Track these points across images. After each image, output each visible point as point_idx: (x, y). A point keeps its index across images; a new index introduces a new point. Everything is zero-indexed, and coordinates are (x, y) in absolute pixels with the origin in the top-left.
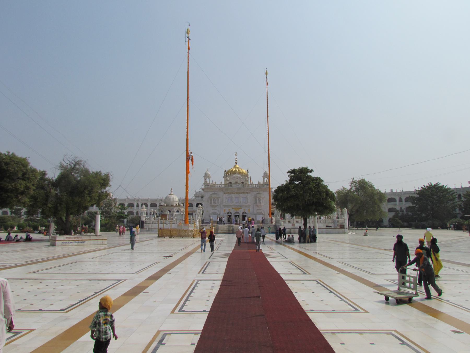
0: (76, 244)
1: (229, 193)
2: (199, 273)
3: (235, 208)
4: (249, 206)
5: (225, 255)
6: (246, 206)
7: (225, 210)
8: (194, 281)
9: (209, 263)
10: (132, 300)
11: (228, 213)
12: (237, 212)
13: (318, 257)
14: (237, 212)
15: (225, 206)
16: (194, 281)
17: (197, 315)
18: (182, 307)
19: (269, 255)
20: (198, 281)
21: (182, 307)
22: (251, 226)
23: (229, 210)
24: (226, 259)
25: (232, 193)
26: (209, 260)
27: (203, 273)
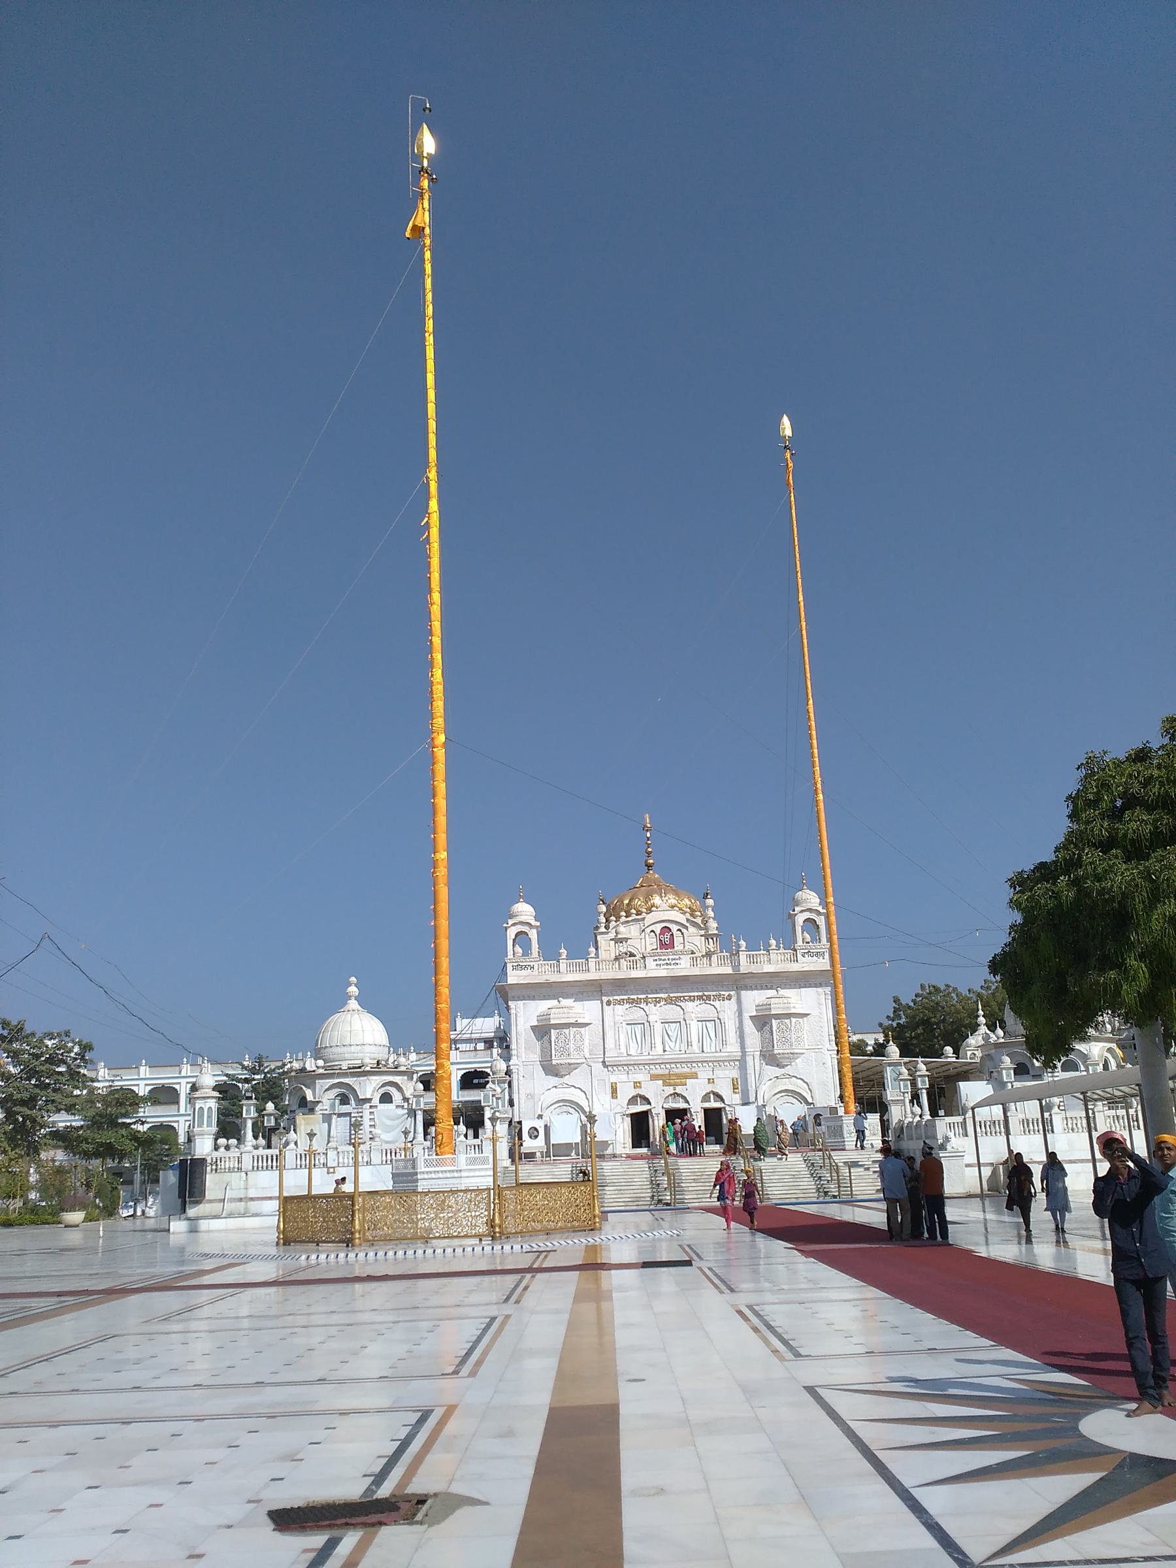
9: (507, 1300)
11: (632, 1101)
23: (637, 1085)
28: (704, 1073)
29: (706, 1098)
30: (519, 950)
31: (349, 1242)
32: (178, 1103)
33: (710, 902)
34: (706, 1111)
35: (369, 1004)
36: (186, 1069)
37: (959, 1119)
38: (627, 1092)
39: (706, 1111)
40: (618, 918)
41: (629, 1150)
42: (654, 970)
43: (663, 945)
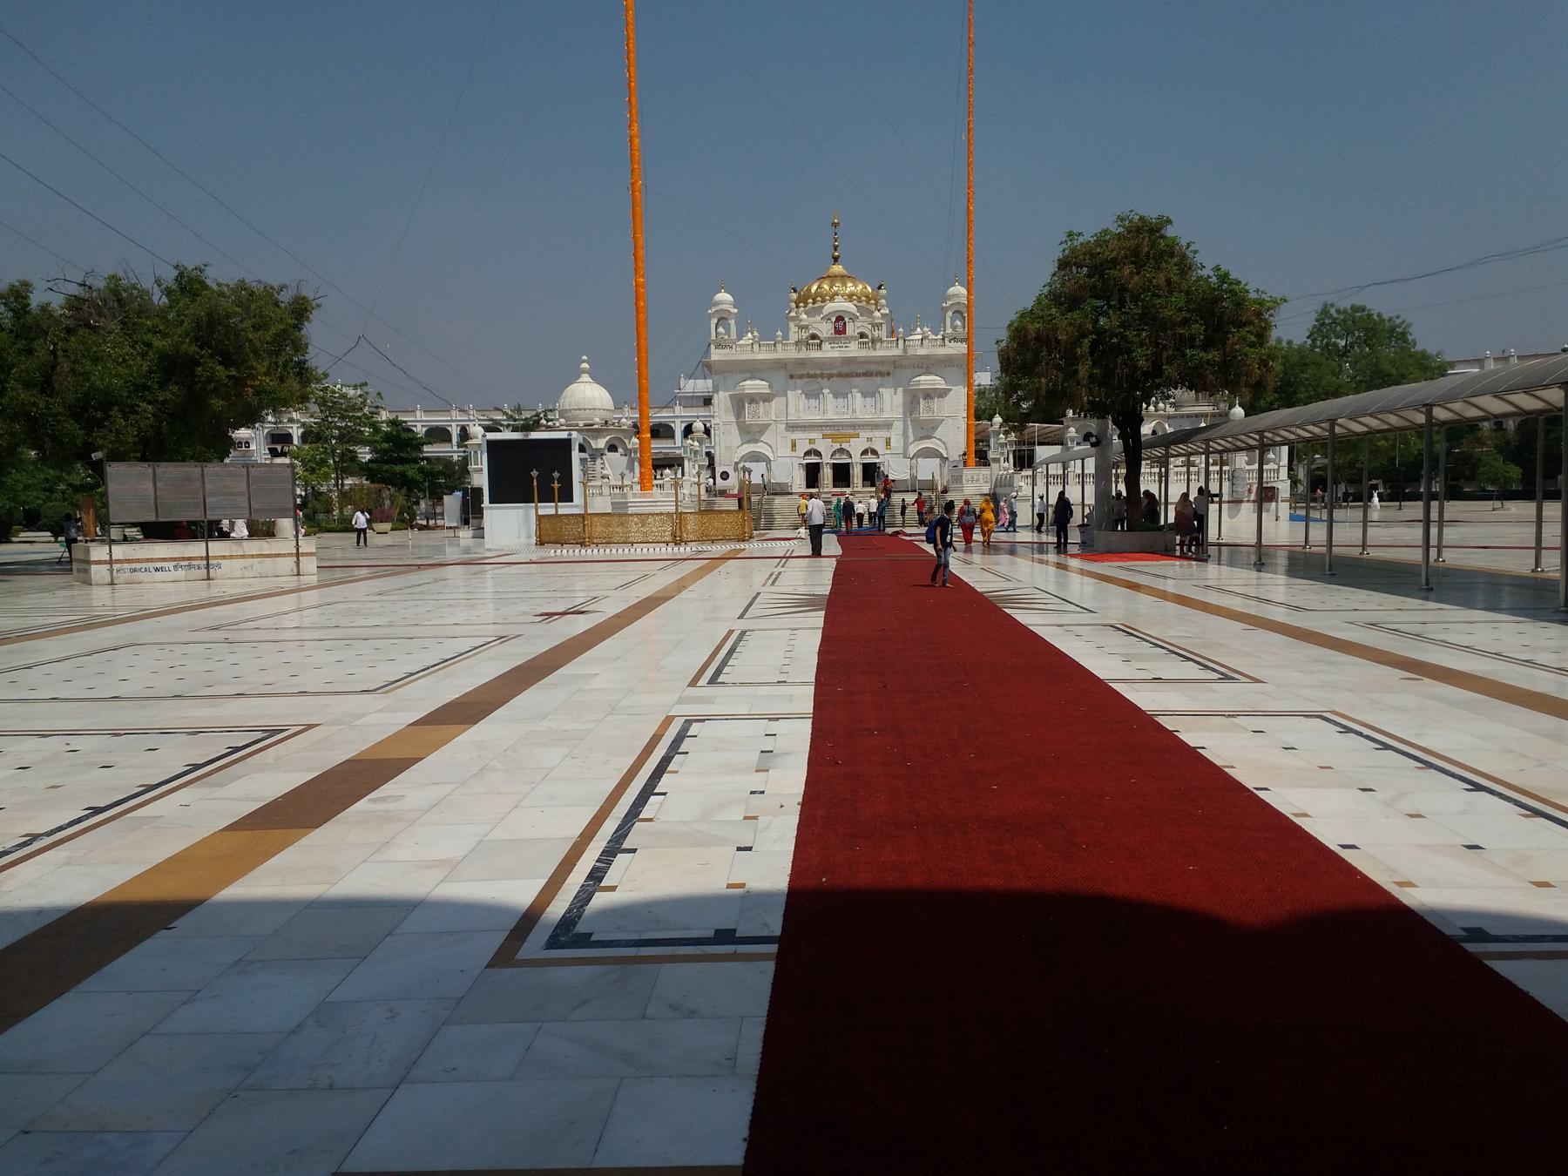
0: (181, 573)
1: (809, 376)
2: (693, 683)
3: (834, 438)
4: (888, 425)
5: (809, 603)
6: (875, 426)
7: (794, 445)
8: (669, 720)
9: (743, 633)
10: (305, 841)
11: (808, 453)
12: (841, 450)
13: (1212, 598)
14: (841, 450)
15: (792, 427)
16: (669, 720)
17: (678, 978)
18: (718, 672)
19: (1010, 600)
20: (688, 723)
21: (718, 672)
22: (1029, 356)
23: (812, 441)
24: (818, 618)
25: (822, 376)
26: (740, 626)
27: (713, 681)
28: (864, 434)
29: (865, 452)
30: (721, 330)
31: (582, 544)
32: (673, 437)
33: (883, 292)
34: (865, 465)
35: (597, 379)
36: (455, 415)
37: (1029, 472)
38: (804, 447)
39: (566, 444)
40: (806, 304)
41: (804, 490)
42: (829, 352)
43: (837, 331)
